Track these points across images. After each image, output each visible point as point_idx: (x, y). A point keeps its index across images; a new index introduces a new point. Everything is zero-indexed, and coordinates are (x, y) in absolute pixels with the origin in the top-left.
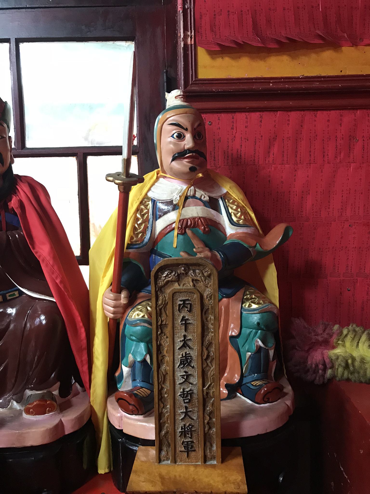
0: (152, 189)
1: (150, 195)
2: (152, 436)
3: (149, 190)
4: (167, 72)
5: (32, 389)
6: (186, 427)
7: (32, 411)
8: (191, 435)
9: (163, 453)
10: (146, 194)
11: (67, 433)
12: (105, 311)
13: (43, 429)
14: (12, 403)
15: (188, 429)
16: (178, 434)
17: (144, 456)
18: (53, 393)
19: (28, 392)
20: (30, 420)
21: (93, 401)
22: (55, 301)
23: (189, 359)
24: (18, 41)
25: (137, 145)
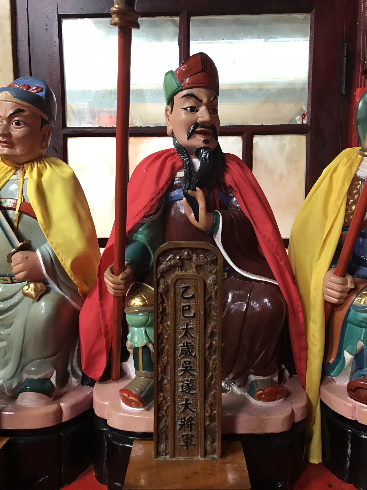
0: (360, 168)
1: (359, 174)
3: (358, 169)
4: (347, 46)
5: (256, 374)
7: (264, 397)
8: (191, 428)
9: (163, 447)
10: (355, 174)
11: (63, 421)
12: (325, 295)
13: (282, 416)
14: (232, 388)
15: (188, 422)
16: (178, 427)
18: (274, 379)
19: (253, 377)
20: (262, 406)
21: (308, 388)
22: (277, 284)
23: (190, 348)
24: (61, 18)
25: (307, 124)
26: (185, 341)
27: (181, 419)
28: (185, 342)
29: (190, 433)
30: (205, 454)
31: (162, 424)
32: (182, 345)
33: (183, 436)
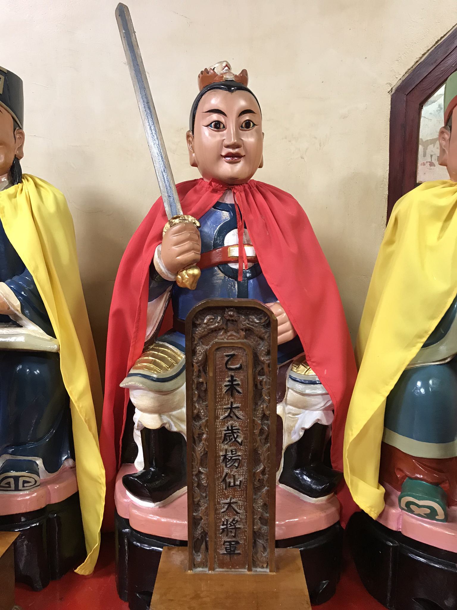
2: (182, 534)
6: (229, 523)
15: (231, 526)
17: (172, 560)
23: (235, 433)
27: (223, 522)
29: (234, 539)
32: (226, 428)
33: (225, 542)
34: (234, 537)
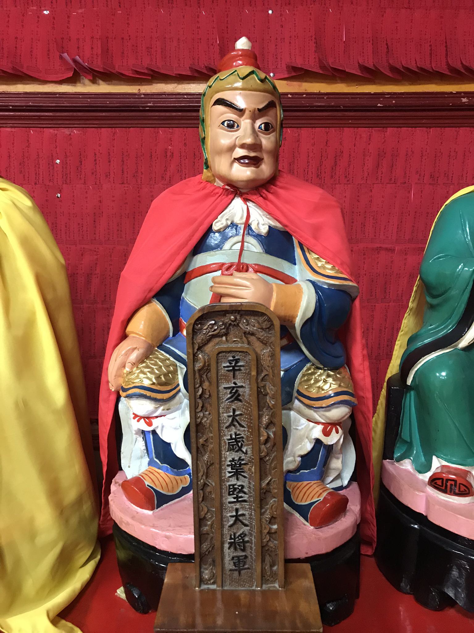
22: (285, 504)
26: (233, 430)
27: (231, 536)
28: (233, 433)
30: (264, 579)
31: (205, 546)
32: (229, 437)
34: (243, 550)
